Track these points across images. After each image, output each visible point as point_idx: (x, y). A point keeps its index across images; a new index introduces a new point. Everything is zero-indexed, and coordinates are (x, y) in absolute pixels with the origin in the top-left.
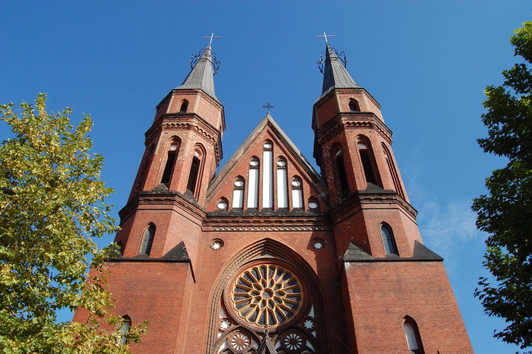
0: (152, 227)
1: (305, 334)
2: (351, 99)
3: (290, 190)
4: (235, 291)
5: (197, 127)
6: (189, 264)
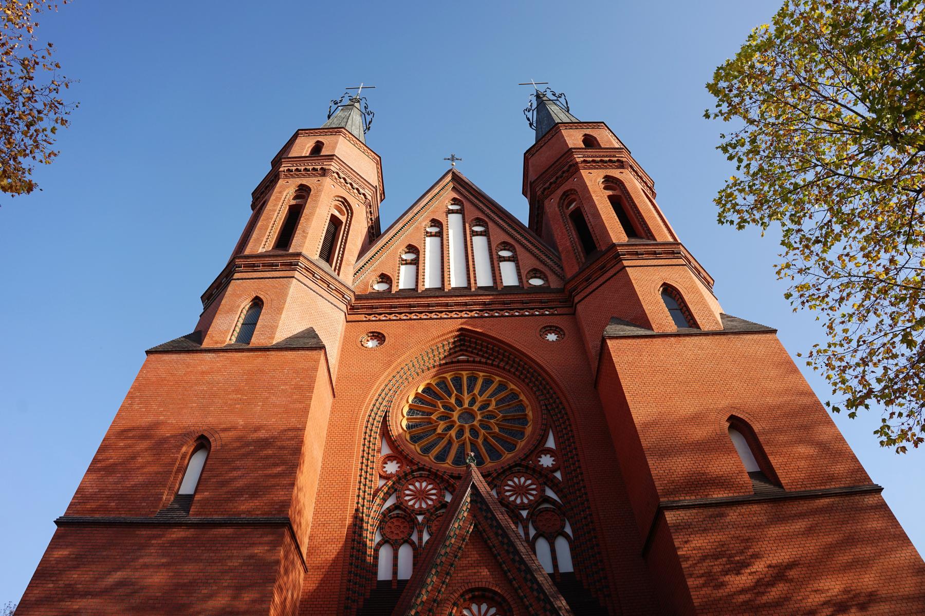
0: (257, 303)
1: (544, 477)
2: (585, 135)
3: (496, 263)
4: (408, 415)
5: (337, 173)
6: (322, 352)
